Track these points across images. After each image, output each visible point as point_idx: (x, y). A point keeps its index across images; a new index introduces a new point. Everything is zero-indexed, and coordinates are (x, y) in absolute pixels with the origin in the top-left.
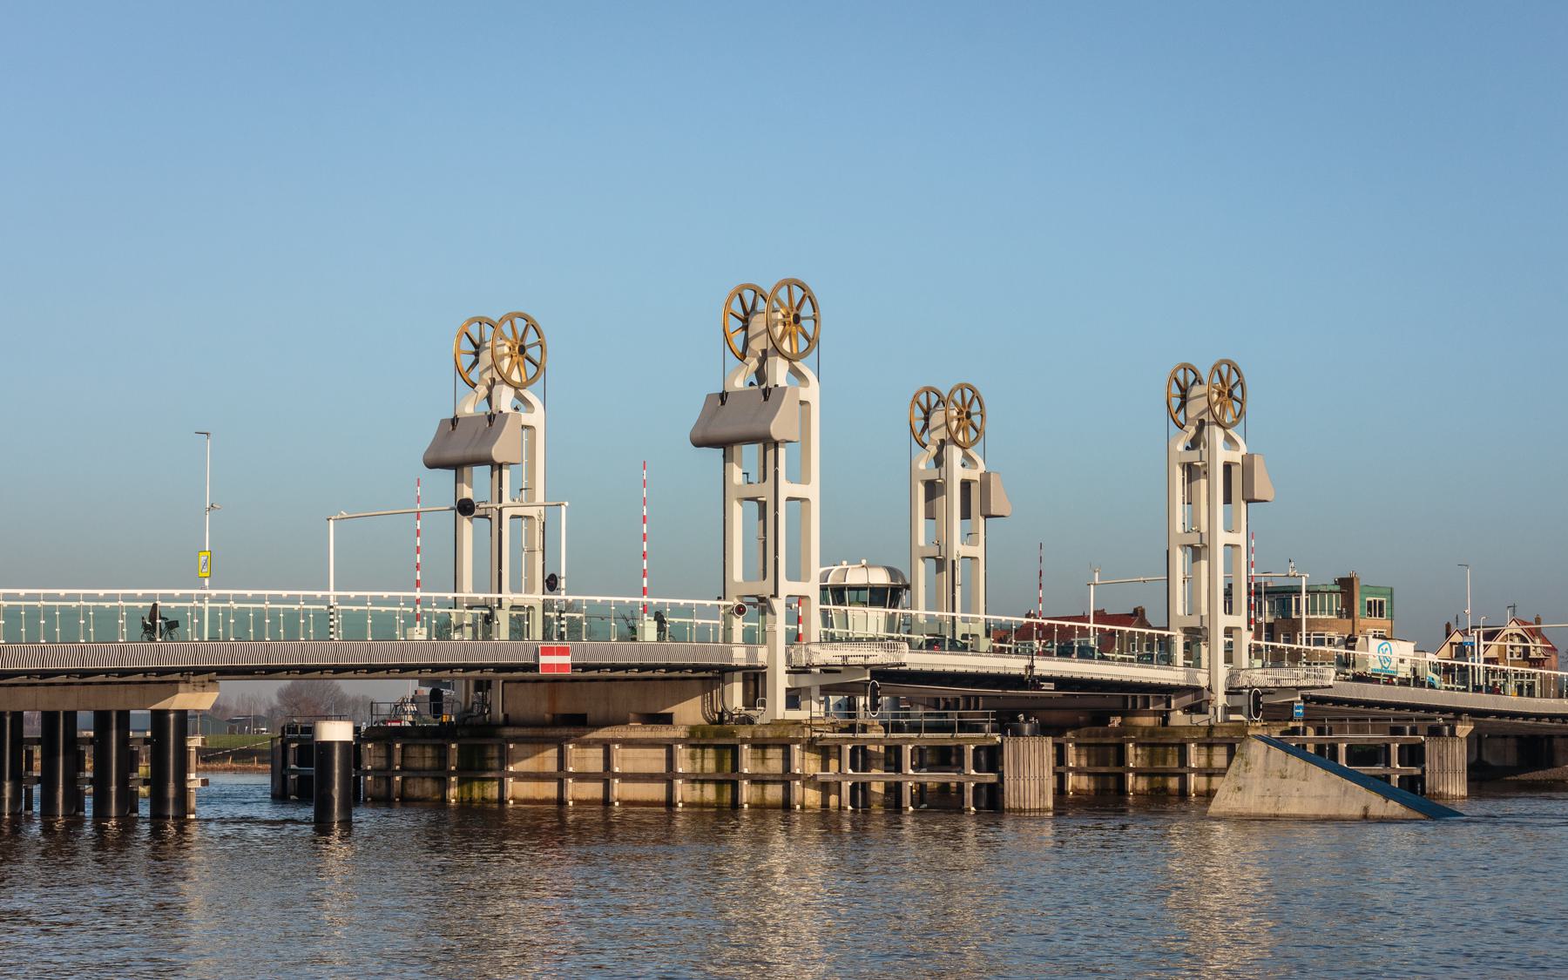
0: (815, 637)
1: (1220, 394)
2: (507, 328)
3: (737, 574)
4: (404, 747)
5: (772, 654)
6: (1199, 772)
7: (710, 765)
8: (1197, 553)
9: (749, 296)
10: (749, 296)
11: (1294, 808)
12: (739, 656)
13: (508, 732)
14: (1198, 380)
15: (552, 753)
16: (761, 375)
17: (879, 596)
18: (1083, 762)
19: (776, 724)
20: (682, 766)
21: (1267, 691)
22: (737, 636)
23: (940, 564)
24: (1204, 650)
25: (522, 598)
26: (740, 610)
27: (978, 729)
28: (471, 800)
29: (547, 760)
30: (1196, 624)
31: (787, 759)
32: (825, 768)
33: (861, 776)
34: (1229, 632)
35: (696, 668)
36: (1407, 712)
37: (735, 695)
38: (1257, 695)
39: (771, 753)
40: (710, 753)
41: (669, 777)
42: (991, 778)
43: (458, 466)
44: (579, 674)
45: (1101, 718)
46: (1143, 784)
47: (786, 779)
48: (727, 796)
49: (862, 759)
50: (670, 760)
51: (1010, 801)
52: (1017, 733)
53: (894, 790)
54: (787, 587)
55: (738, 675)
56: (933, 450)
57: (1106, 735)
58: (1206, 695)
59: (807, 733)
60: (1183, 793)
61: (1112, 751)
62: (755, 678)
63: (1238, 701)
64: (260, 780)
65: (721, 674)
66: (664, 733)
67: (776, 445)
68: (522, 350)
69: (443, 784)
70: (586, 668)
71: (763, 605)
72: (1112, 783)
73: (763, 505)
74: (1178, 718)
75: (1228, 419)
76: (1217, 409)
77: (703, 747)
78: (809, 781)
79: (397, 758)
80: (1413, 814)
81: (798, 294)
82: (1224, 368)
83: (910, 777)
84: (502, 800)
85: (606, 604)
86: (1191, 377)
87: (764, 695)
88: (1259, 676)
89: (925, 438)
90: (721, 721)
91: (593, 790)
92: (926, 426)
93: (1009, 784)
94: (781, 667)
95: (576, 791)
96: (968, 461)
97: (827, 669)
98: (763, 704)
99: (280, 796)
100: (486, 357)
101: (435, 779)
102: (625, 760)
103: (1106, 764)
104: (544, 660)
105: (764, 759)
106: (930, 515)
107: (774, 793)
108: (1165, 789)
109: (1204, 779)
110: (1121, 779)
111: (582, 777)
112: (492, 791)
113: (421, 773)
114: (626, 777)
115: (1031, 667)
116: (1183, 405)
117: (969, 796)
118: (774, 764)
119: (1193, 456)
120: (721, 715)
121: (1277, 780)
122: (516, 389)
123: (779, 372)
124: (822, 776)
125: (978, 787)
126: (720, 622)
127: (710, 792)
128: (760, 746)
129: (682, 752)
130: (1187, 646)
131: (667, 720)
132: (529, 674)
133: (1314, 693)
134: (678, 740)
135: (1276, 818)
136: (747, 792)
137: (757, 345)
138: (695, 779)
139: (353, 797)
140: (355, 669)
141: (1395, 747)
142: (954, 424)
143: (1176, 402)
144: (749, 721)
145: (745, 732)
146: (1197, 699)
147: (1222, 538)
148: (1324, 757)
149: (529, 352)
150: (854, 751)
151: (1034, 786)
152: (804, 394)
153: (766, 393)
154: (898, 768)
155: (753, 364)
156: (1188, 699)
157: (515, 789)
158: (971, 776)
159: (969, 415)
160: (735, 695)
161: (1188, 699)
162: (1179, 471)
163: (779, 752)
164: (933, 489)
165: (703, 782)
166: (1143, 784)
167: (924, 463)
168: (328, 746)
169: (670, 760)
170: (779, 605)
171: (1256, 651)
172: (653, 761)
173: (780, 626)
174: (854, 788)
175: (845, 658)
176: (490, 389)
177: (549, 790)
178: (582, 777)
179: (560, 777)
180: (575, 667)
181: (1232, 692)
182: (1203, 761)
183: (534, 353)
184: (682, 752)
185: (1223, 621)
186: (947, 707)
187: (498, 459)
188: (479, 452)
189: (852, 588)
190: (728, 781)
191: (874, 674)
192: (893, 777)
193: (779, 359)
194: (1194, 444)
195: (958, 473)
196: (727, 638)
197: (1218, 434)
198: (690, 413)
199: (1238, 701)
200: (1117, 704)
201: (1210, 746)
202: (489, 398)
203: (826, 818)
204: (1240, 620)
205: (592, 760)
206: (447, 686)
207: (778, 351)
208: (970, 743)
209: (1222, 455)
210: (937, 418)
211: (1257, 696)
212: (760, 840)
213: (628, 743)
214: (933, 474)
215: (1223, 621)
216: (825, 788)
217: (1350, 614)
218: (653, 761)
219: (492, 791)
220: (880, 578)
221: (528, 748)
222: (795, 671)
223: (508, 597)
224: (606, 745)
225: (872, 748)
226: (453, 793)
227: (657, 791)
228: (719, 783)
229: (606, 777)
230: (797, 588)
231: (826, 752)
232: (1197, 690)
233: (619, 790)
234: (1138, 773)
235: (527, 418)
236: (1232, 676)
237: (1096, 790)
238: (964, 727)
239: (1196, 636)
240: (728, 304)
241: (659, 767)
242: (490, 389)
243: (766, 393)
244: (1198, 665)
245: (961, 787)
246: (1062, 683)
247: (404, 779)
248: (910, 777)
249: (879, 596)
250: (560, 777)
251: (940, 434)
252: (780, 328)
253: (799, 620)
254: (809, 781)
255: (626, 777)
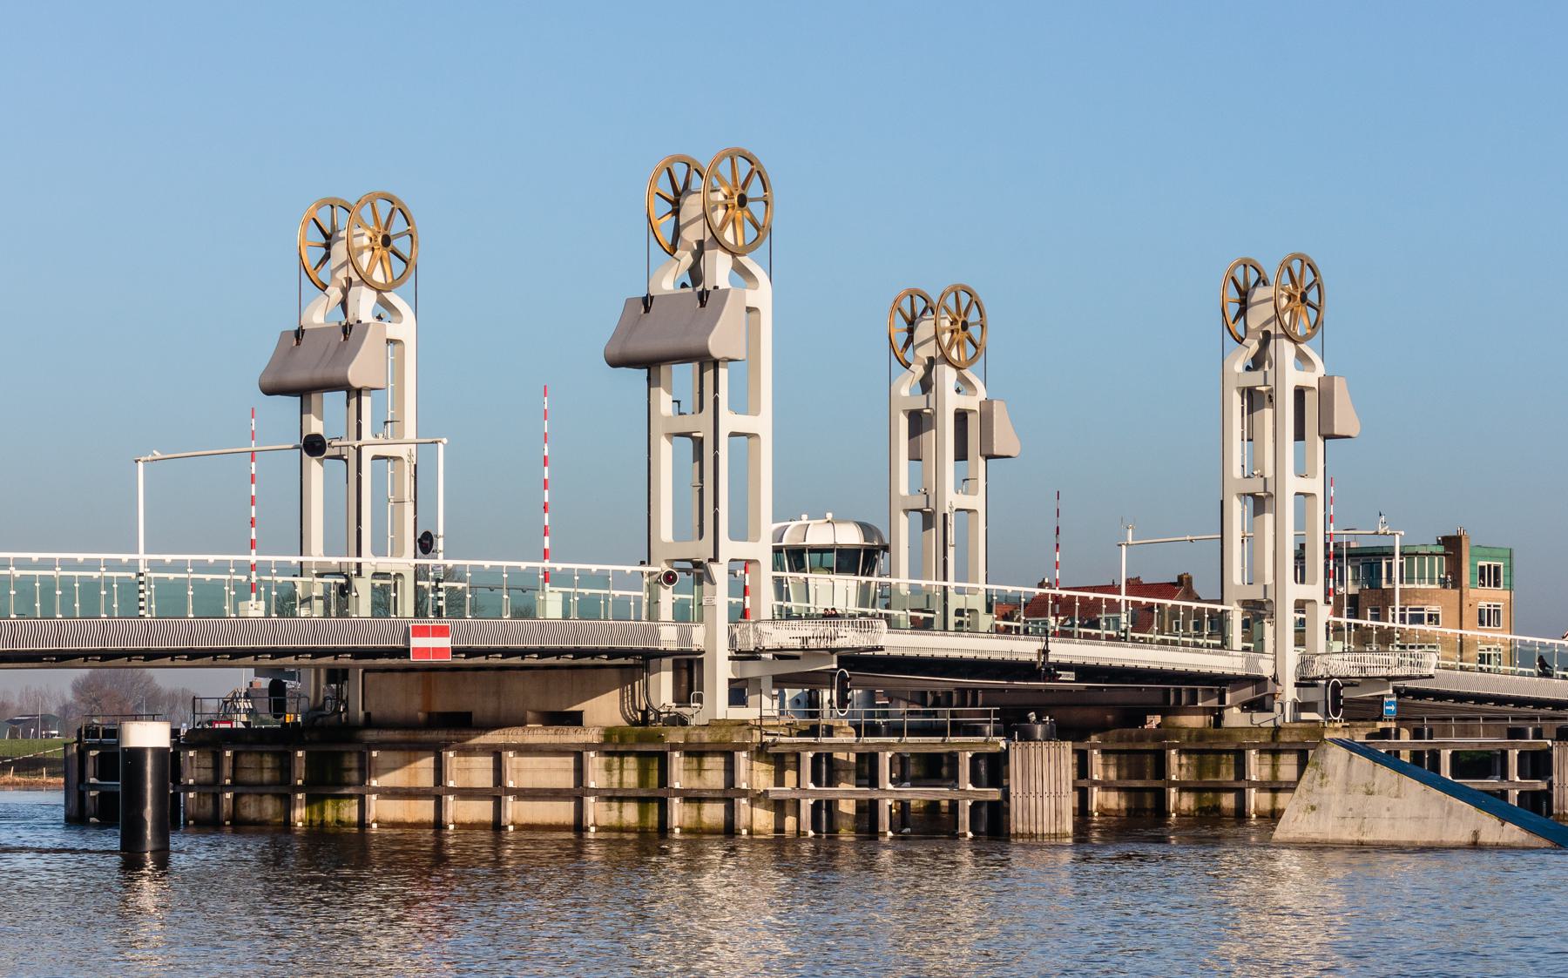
0: (766, 613)
1: (1290, 297)
2: (366, 212)
3: (665, 530)
4: (236, 755)
5: (711, 636)
6: (1261, 786)
7: (631, 778)
8: (1260, 504)
9: (680, 172)
10: (680, 172)
11: (1382, 832)
12: (669, 637)
13: (371, 735)
14: (1262, 281)
15: (428, 762)
16: (696, 274)
17: (849, 560)
18: (1112, 774)
19: (714, 724)
20: (597, 776)
21: (1350, 682)
22: (666, 612)
23: (928, 519)
24: (1268, 630)
25: (388, 564)
26: (670, 578)
27: (976, 731)
28: (323, 823)
29: (421, 772)
30: (1259, 596)
31: (730, 769)
32: (779, 782)
33: (827, 792)
34: (1300, 606)
35: (613, 653)
36: (1529, 709)
37: (663, 688)
38: (1336, 687)
39: (709, 762)
40: (631, 763)
41: (578, 794)
42: (994, 794)
43: (304, 393)
44: (462, 661)
45: (1133, 716)
46: (1188, 802)
47: (729, 796)
48: (653, 819)
49: (826, 769)
50: (580, 771)
51: (1017, 824)
52: (1027, 736)
53: (868, 810)
54: (730, 549)
55: (667, 662)
56: (919, 370)
57: (1141, 739)
58: (1270, 688)
59: (756, 737)
60: (1241, 813)
61: (1149, 760)
62: (689, 667)
63: (1312, 695)
64: (50, 797)
65: (647, 660)
66: (571, 736)
67: (716, 364)
68: (386, 241)
69: (288, 804)
70: (471, 653)
71: (699, 572)
72: (1149, 801)
73: (699, 443)
74: (1235, 717)
75: (1300, 331)
76: (1287, 317)
77: (622, 755)
78: (757, 798)
79: (227, 769)
80: (1544, 843)
81: (743, 168)
82: (1296, 266)
83: (889, 795)
84: (362, 824)
85: (496, 571)
86: (1253, 277)
87: (701, 688)
88: (1339, 662)
89: (908, 356)
90: (645, 721)
91: (480, 811)
92: (910, 340)
93: (1016, 803)
94: (723, 651)
95: (458, 811)
96: (964, 385)
97: (781, 655)
98: (700, 699)
99: (76, 819)
100: (339, 251)
101: (276, 796)
102: (523, 772)
103: (1141, 777)
104: (416, 642)
105: (700, 770)
106: (915, 456)
107: (713, 813)
108: (1217, 808)
109: (1268, 796)
110: (1161, 795)
111: (466, 793)
112: (350, 812)
113: (259, 789)
114: (524, 794)
115: (1046, 652)
116: (1242, 312)
117: (965, 816)
118: (714, 776)
119: (1255, 379)
120: (645, 714)
121: (1360, 796)
122: (379, 291)
123: (719, 269)
124: (776, 792)
125: (976, 806)
126: (644, 594)
127: (631, 813)
128: (696, 753)
129: (594, 762)
130: (1246, 624)
131: (576, 719)
132: (395, 661)
133: (1409, 684)
134: (589, 746)
135: (1360, 847)
136: (679, 813)
137: (692, 235)
138: (614, 797)
139: (170, 819)
140: (214, 654)
141: (1513, 755)
142: (946, 337)
143: (1233, 309)
144: (681, 721)
145: (676, 736)
146: (1259, 693)
147: (1292, 484)
148: (1422, 767)
149: (395, 243)
150: (816, 760)
151: (1048, 803)
152: (752, 298)
153: (703, 297)
154: (874, 782)
155: (686, 259)
156: (1248, 693)
157: (381, 810)
158: (967, 791)
159: (965, 326)
160: (663, 688)
161: (1248, 693)
162: (1237, 397)
163: (719, 762)
164: (919, 422)
165: (621, 800)
166: (1188, 802)
167: (906, 388)
168: (138, 753)
169: (580, 771)
170: (719, 572)
171: (1336, 631)
172: (558, 772)
173: (721, 597)
174: (816, 807)
175: (805, 640)
176: (345, 291)
177: (423, 810)
178: (466, 793)
179: (437, 794)
180: (456, 651)
181: (1303, 683)
182: (1266, 772)
183: (402, 245)
184: (594, 762)
185: (1294, 591)
186: (936, 703)
187: (716, 352)
188: (690, 343)
189: (813, 550)
190: (655, 798)
191: (843, 661)
192: (866, 793)
193: (364, 289)
194: (1257, 363)
195: (951, 401)
196: (653, 615)
197: (1288, 350)
198: (260, 354)
199: (1312, 695)
200: (1157, 698)
201: (1275, 753)
202: (344, 304)
203: (779, 843)
204: (1314, 590)
205: (478, 772)
206: (292, 676)
207: (717, 242)
208: (965, 749)
209: (1293, 377)
210: (924, 330)
211: (1336, 688)
212: (693, 867)
213: (524, 750)
214: (919, 403)
215: (1294, 591)
216: (779, 807)
217: (1457, 583)
218: (558, 772)
219: (350, 812)
220: (850, 536)
221: (397, 756)
222: (740, 656)
223: (370, 561)
224: (497, 753)
225: (840, 756)
226: (300, 814)
227: (562, 812)
228: (643, 801)
229: (496, 793)
230: (743, 550)
231: (780, 761)
232: (1259, 681)
233: (514, 811)
234: (1183, 788)
235: (392, 330)
236: (1304, 663)
237: (1128, 810)
238: (958, 729)
239: (1257, 611)
240: (654, 180)
241: (566, 780)
242: (345, 291)
243: (703, 297)
244: (1260, 649)
245: (954, 805)
246: (1085, 672)
247: (236, 797)
248: (889, 795)
249: (849, 560)
250: (437, 794)
251: (928, 351)
252: (721, 213)
253: (745, 591)
254: (757, 798)
255: (524, 794)
